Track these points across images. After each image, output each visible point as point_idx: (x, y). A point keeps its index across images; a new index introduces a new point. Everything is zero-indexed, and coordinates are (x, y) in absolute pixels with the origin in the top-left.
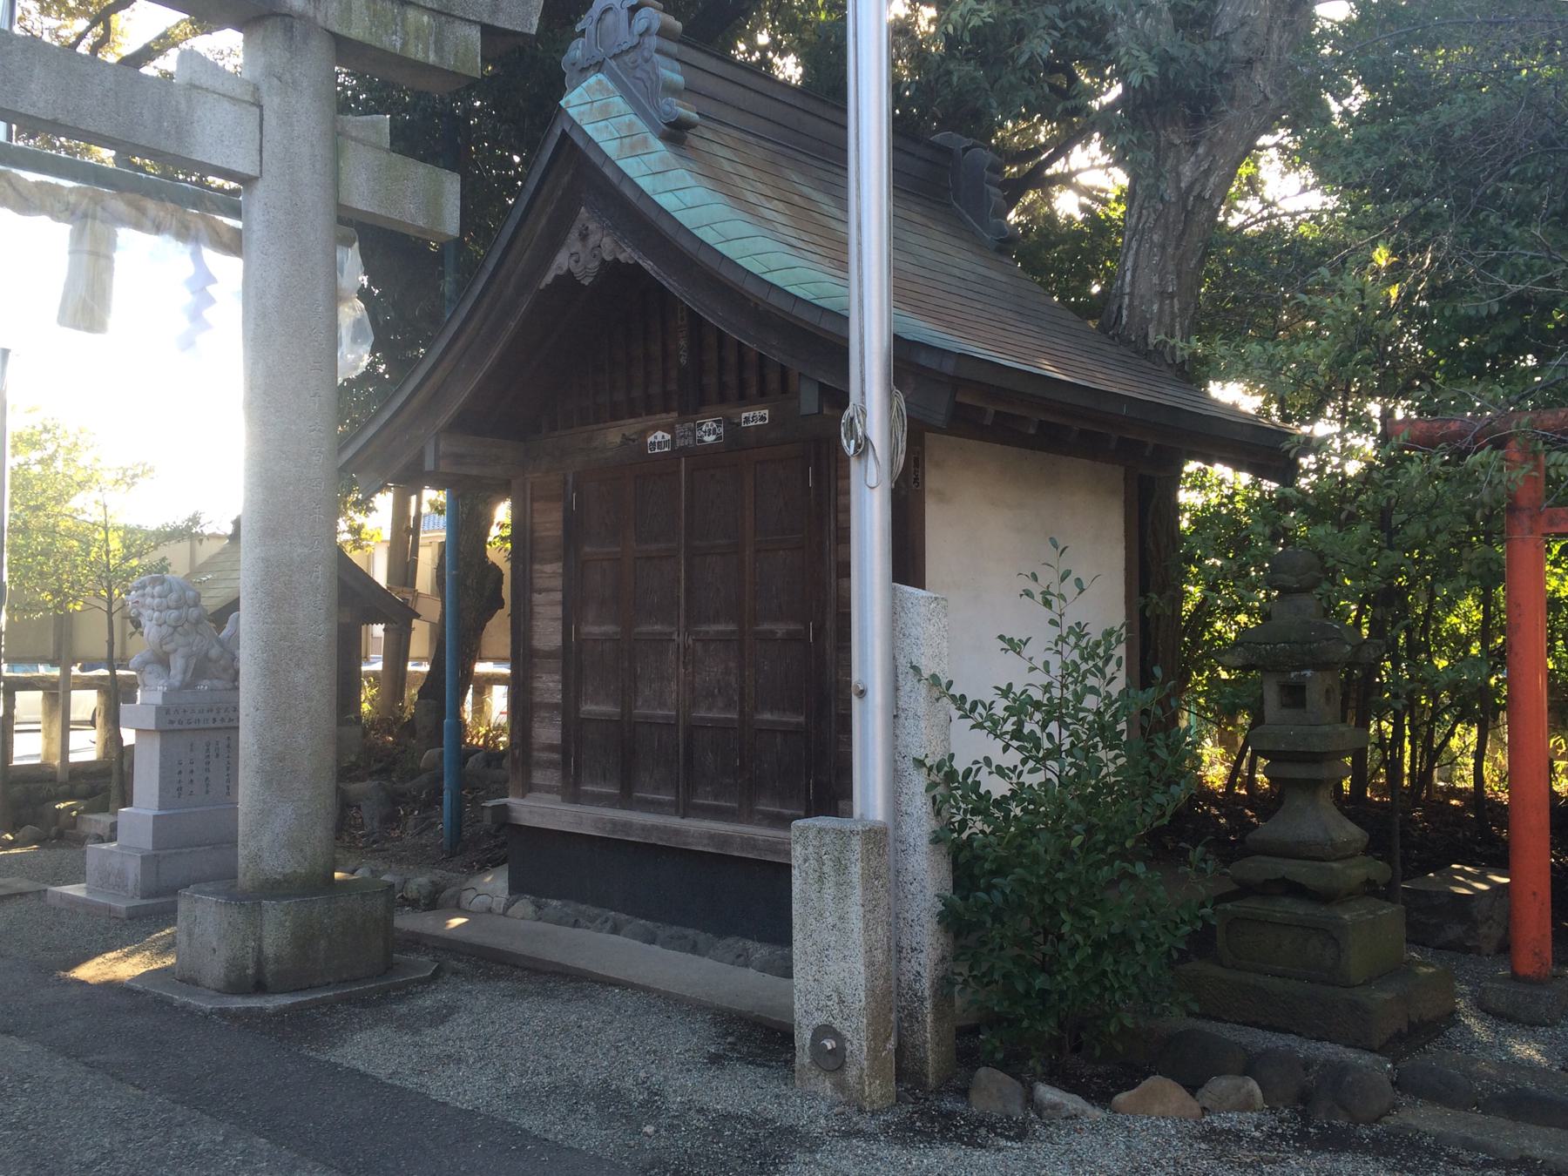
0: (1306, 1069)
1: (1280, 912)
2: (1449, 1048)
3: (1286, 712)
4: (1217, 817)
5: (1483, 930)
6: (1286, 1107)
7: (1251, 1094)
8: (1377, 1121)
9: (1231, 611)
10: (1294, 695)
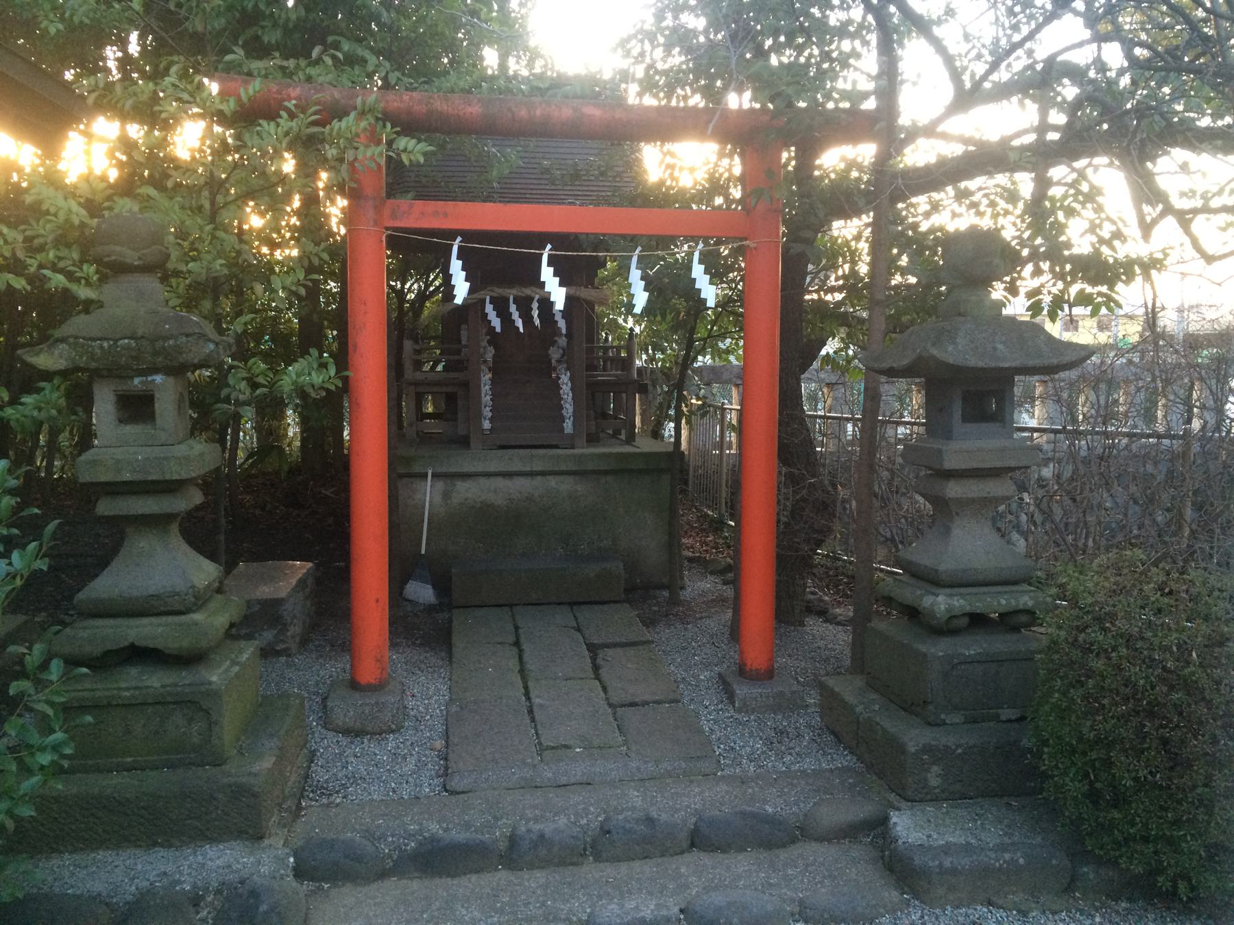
1: (128, 689)
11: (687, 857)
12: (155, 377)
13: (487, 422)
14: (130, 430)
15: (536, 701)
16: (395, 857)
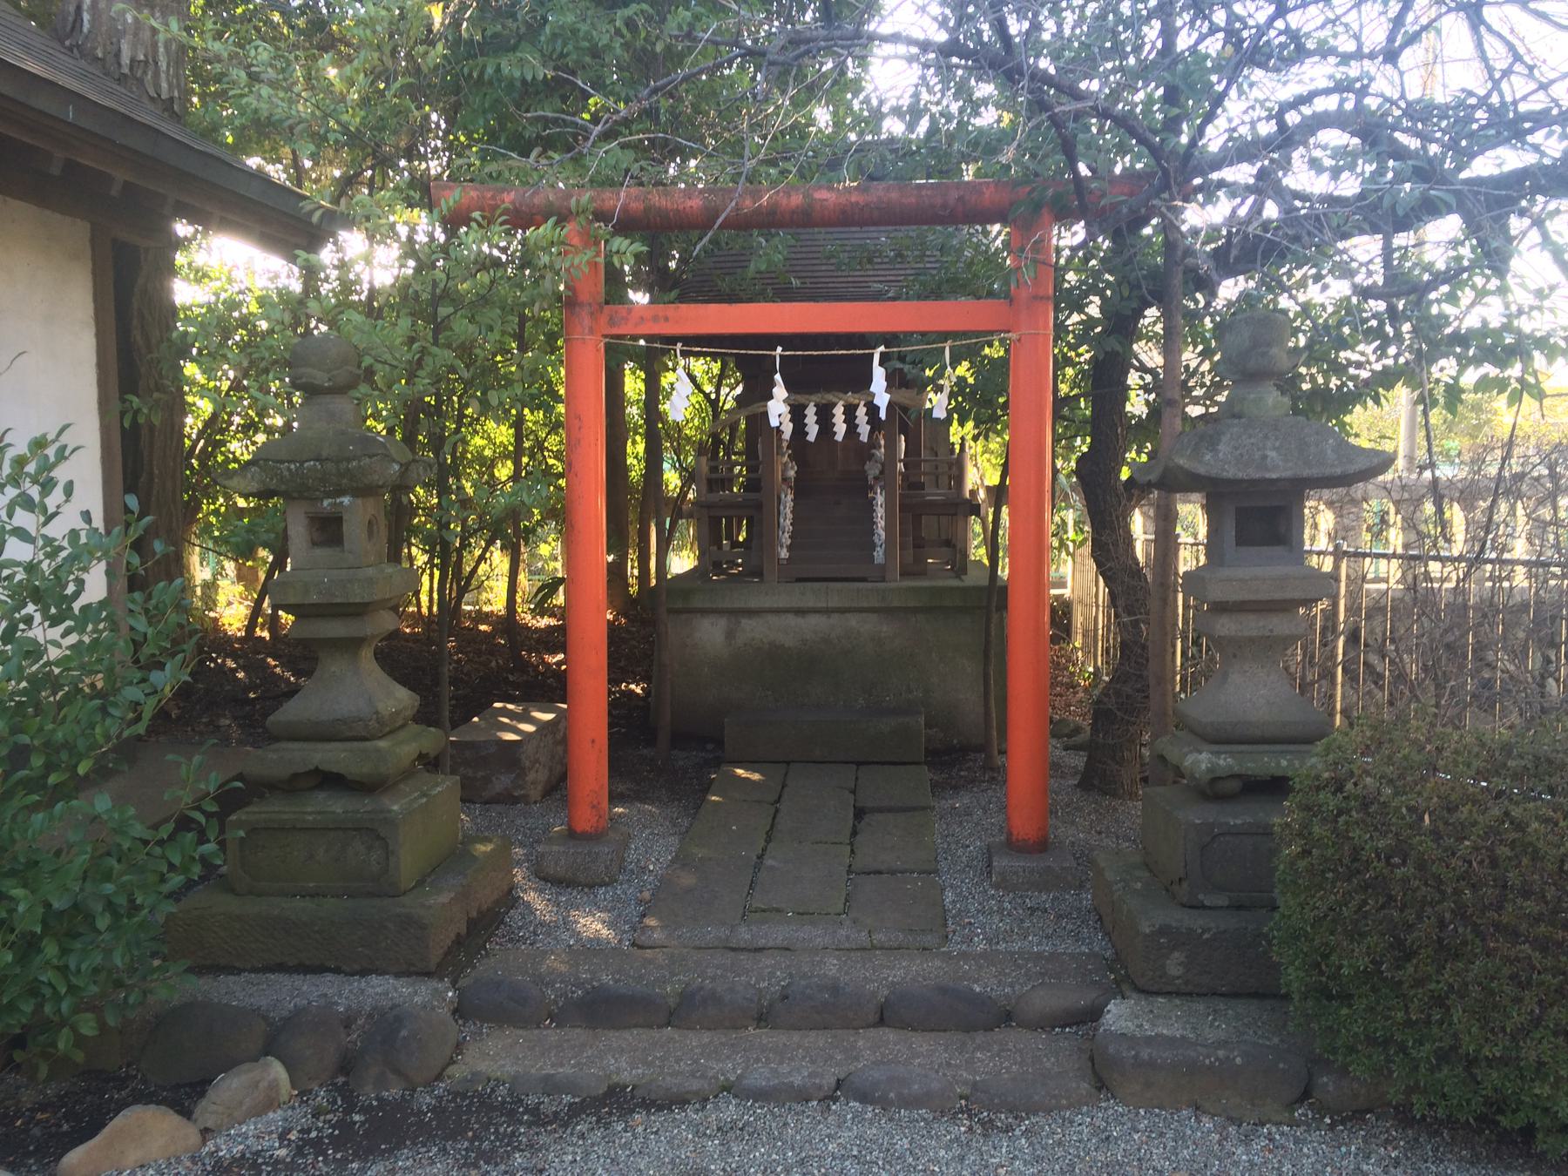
0: (347, 1027)
2: (511, 940)
3: (319, 552)
4: (234, 671)
5: (531, 776)
6: (321, 1086)
7: (274, 1086)
8: (439, 1077)
9: (249, 428)
10: (328, 530)
11: (872, 1032)
12: (342, 499)
13: (785, 550)
14: (320, 552)
15: (769, 862)
16: (561, 1004)
